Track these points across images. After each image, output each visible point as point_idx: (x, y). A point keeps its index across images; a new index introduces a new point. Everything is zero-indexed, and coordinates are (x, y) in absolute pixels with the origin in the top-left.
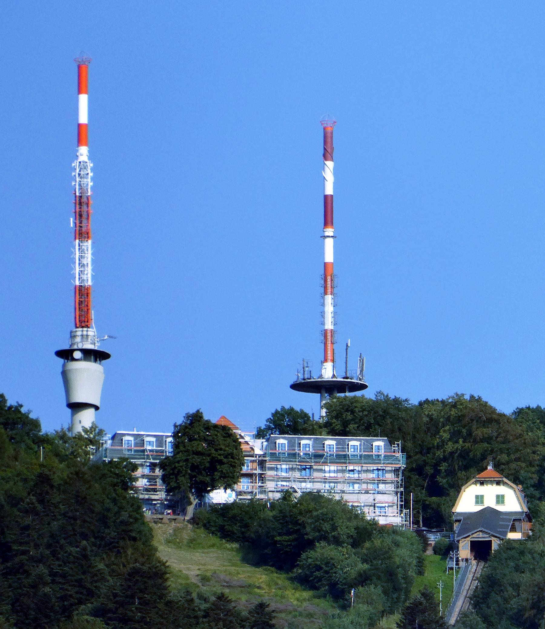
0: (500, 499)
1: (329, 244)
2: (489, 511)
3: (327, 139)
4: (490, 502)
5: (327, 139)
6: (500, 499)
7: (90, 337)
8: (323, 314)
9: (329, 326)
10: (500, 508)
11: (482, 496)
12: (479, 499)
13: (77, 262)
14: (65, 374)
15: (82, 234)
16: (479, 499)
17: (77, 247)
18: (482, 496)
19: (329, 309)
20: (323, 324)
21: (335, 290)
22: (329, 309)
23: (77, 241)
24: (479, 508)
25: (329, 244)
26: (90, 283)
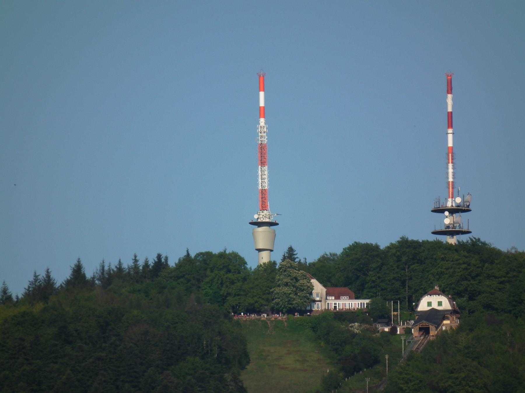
0: (440, 304)
1: (450, 137)
2: (433, 309)
3: (450, 83)
4: (435, 306)
5: (450, 83)
6: (440, 304)
7: (263, 216)
8: (447, 173)
9: (451, 180)
10: (440, 308)
11: (431, 302)
12: (429, 304)
13: (260, 177)
14: (253, 233)
15: (263, 164)
16: (429, 304)
17: (260, 169)
18: (431, 302)
19: (451, 171)
20: (448, 178)
21: (454, 161)
22: (451, 171)
23: (260, 166)
24: (430, 308)
25: (450, 137)
26: (266, 188)
